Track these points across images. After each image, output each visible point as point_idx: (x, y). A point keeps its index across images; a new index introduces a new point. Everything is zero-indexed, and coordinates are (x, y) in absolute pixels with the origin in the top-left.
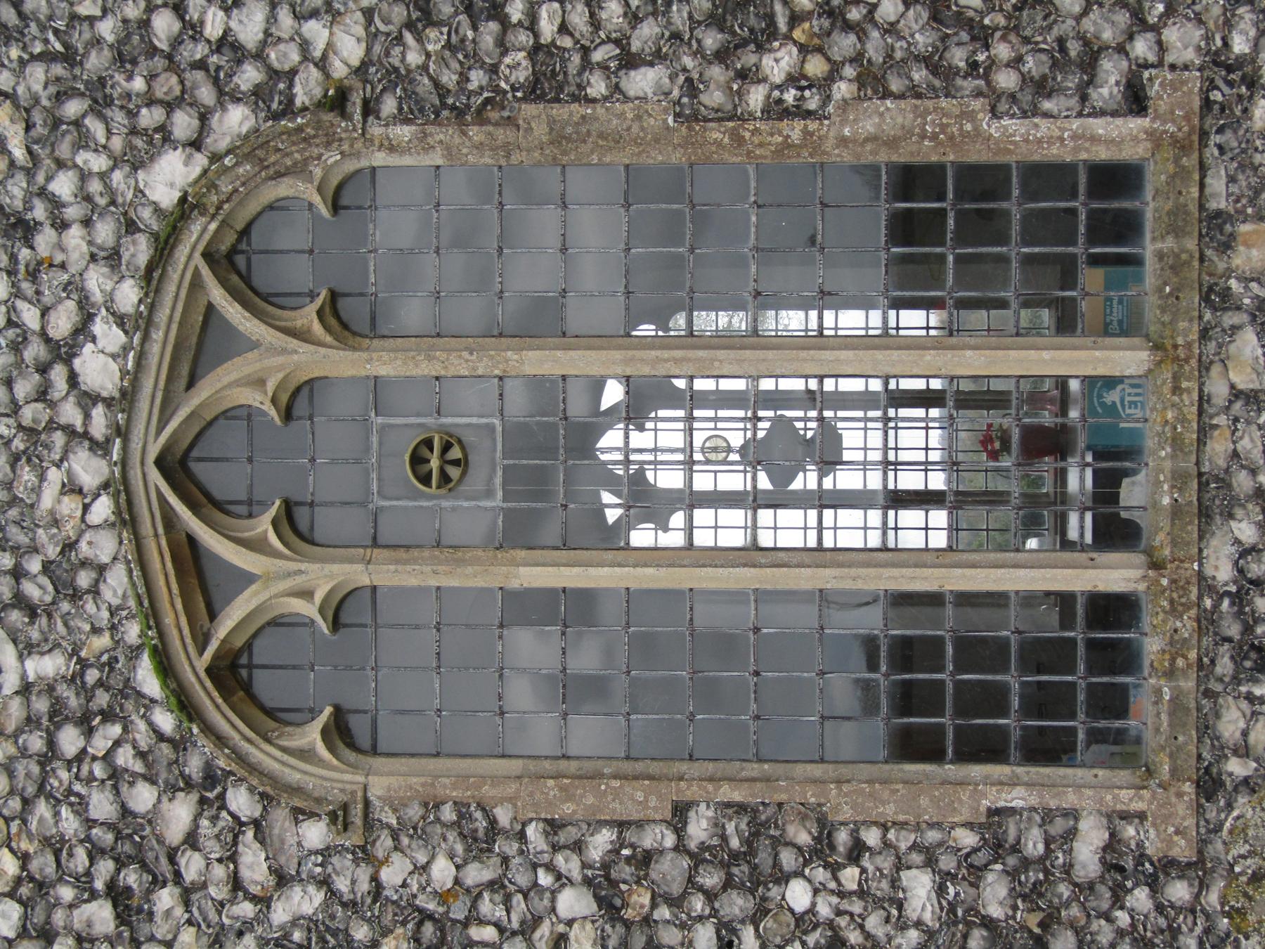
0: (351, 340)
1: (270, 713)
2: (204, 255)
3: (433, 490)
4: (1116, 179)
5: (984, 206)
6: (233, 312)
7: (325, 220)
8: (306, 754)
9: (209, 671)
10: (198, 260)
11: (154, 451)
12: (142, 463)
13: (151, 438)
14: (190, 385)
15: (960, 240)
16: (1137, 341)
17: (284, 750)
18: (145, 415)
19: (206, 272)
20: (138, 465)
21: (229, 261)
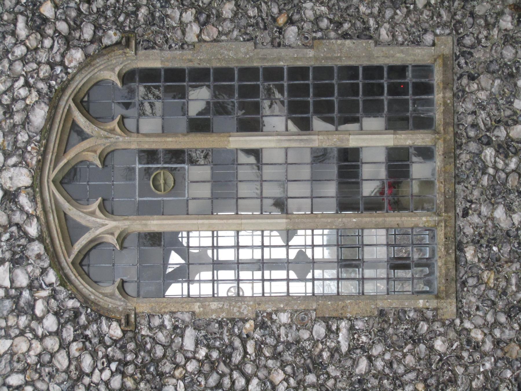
0: (130, 134)
1: (96, 282)
2: (73, 100)
3: (162, 193)
4: (424, 70)
5: (371, 82)
6: (81, 120)
7: (119, 89)
8: (92, 214)
9: (73, 263)
10: (71, 102)
11: (53, 176)
12: (48, 182)
13: (51, 172)
14: (65, 152)
15: (414, 94)
16: (429, 131)
17: (101, 293)
18: (54, 140)
19: (73, 105)
20: (68, 96)
21: (83, 105)
